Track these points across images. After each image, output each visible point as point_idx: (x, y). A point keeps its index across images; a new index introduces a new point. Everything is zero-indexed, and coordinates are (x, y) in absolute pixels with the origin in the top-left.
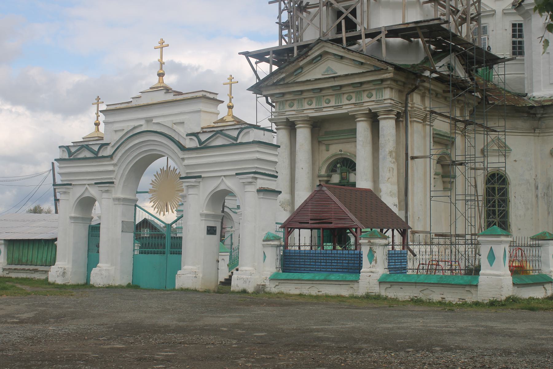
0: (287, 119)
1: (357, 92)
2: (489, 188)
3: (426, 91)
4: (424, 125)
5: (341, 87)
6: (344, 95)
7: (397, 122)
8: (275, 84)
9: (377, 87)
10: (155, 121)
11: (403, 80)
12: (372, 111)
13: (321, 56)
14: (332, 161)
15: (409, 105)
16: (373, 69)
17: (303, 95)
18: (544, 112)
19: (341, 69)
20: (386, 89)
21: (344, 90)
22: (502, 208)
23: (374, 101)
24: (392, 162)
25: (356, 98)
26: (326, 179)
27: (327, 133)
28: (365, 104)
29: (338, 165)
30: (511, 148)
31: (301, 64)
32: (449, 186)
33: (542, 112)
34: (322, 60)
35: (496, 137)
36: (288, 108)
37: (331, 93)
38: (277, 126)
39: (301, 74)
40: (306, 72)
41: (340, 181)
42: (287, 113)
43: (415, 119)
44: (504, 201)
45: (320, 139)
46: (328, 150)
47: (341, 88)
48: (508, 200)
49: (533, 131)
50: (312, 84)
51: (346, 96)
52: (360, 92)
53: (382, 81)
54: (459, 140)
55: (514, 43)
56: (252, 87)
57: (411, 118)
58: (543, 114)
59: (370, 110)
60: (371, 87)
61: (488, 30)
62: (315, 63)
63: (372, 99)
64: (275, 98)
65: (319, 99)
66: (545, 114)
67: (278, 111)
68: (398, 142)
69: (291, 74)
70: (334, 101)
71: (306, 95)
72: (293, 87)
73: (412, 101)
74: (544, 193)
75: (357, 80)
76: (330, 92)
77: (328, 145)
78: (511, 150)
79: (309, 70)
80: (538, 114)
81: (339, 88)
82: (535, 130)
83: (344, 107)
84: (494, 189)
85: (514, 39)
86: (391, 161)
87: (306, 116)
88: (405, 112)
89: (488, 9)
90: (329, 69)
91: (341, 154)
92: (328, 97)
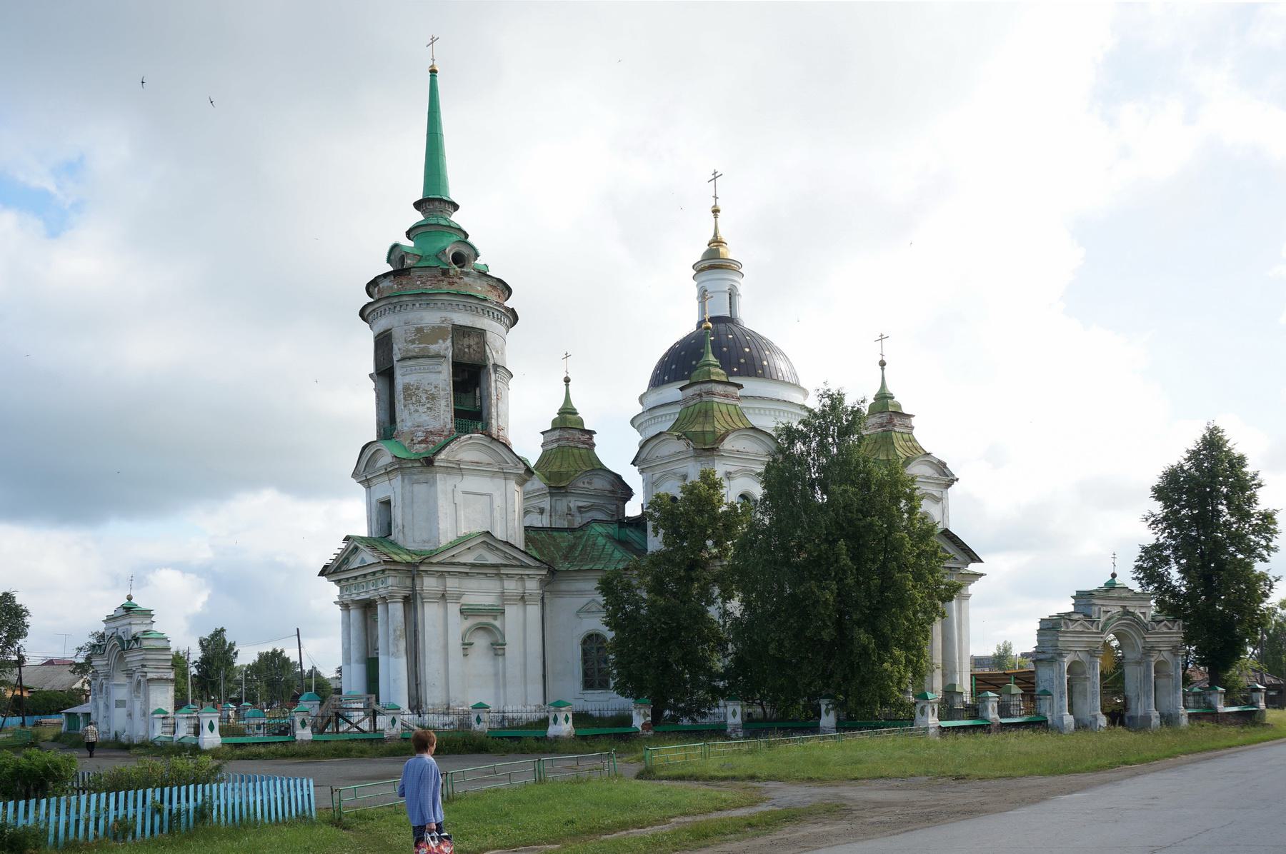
54: (512, 612)
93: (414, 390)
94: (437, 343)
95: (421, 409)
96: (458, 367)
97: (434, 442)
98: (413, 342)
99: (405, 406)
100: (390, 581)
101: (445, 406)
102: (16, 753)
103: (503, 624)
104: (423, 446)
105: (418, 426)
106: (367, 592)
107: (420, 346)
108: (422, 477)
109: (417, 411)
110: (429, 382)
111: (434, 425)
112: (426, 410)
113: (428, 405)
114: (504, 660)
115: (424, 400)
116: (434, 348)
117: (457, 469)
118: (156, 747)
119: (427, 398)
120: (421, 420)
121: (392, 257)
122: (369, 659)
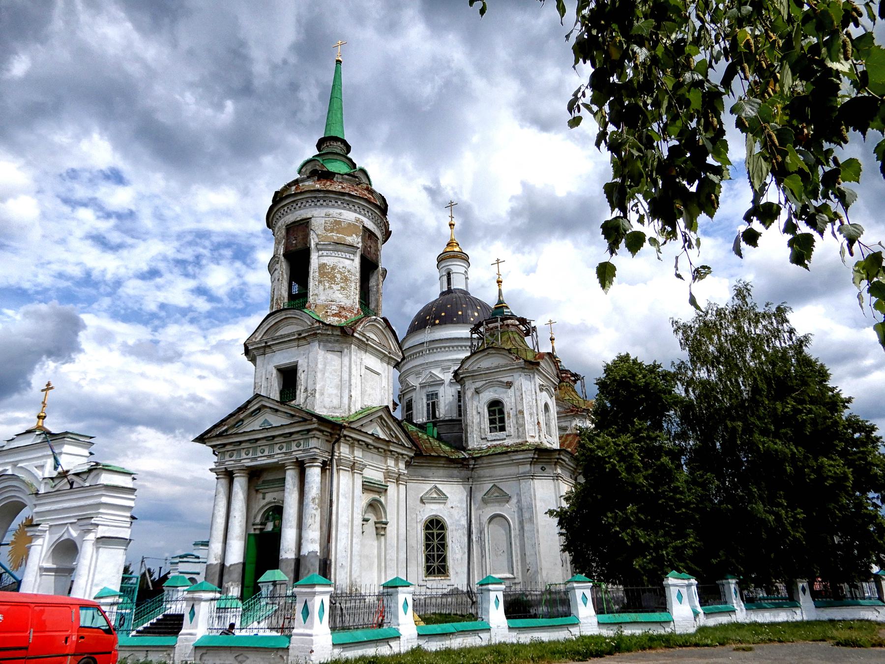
0: (225, 468)
5: (274, 437)
8: (218, 436)
9: (305, 437)
10: (20, 465)
13: (259, 409)
16: (301, 420)
19: (276, 420)
30: (448, 495)
31: (241, 417)
42: (227, 463)
44: (443, 546)
45: (257, 488)
46: (264, 498)
47: (273, 439)
52: (290, 441)
53: (309, 431)
54: (392, 488)
56: (197, 438)
57: (337, 466)
58: (474, 465)
59: (297, 459)
63: (300, 448)
68: (322, 489)
69: (233, 426)
71: (243, 445)
73: (339, 449)
75: (287, 431)
76: (264, 442)
77: (264, 494)
83: (276, 456)
92: (263, 447)
95: (335, 287)
96: (363, 259)
97: (346, 317)
99: (320, 282)
100: (313, 443)
103: (386, 500)
104: (337, 319)
106: (269, 457)
108: (337, 347)
109: (330, 288)
111: (346, 302)
114: (385, 540)
116: (350, 240)
117: (364, 346)
119: (341, 279)
121: (303, 170)
122: (249, 535)
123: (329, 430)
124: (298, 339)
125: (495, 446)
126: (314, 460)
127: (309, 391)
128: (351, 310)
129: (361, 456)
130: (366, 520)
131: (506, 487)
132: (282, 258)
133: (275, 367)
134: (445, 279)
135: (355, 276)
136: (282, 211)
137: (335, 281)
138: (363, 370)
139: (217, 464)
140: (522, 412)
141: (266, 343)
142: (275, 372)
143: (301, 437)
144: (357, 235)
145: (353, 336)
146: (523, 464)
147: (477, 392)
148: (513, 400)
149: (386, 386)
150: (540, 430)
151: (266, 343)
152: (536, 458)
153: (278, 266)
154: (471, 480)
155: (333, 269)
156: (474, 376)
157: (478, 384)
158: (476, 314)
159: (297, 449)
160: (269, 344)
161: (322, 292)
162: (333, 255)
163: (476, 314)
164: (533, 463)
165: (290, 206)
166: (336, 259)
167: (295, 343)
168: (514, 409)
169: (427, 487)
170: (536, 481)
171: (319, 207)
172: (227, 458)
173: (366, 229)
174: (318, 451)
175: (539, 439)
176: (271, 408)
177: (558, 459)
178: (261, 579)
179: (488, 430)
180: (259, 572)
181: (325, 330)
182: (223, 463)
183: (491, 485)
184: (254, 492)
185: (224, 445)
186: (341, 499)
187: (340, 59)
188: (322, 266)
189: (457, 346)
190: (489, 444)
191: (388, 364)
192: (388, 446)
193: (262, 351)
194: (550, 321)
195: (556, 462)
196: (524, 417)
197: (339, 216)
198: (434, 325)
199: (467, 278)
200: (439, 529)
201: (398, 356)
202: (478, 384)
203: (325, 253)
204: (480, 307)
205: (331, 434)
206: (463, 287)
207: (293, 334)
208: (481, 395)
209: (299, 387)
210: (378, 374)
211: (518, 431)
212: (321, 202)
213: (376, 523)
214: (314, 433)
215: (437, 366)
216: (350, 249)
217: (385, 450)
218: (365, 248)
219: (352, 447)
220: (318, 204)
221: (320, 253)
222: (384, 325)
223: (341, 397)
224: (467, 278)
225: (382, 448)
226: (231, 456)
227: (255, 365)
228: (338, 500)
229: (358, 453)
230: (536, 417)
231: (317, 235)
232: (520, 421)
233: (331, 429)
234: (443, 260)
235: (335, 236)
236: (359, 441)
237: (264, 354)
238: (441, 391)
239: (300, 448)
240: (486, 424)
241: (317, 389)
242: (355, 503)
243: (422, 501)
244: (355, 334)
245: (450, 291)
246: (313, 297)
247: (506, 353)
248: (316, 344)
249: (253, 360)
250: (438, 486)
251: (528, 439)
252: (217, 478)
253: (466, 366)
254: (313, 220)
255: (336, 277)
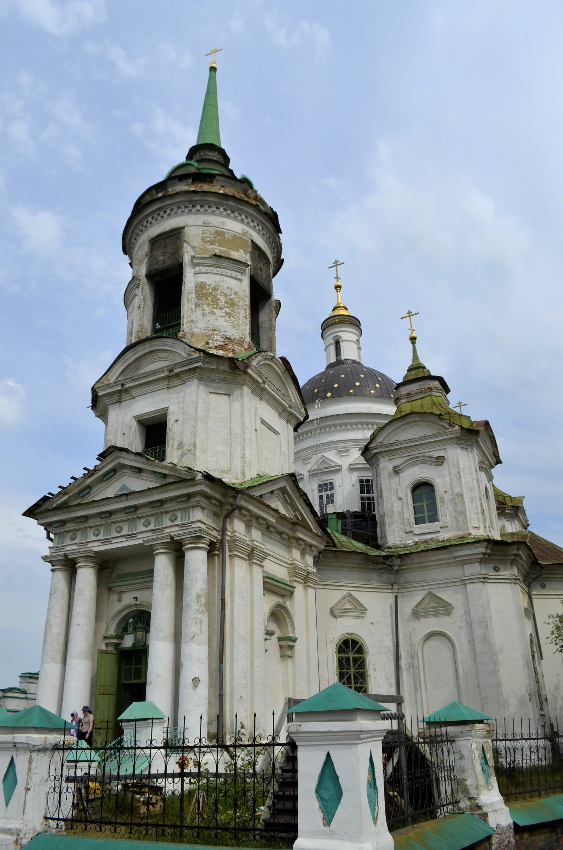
0: (65, 555)
1: (157, 514)
2: (342, 658)
3: (252, 519)
4: (251, 564)
6: (141, 520)
7: (210, 554)
9: (183, 506)
11: (219, 497)
12: (175, 539)
14: (126, 614)
15: (228, 533)
17: (88, 522)
18: (403, 563)
20: (195, 509)
21: (140, 512)
22: (360, 684)
23: (178, 525)
24: (200, 611)
25: (155, 522)
26: (115, 641)
27: (121, 577)
28: (167, 530)
29: (131, 620)
30: (367, 607)
32: (289, 653)
33: (399, 563)
34: (116, 476)
35: (348, 593)
36: (68, 542)
37: (124, 518)
38: (53, 566)
39: (90, 495)
40: (96, 493)
41: (134, 644)
42: (67, 548)
43: (236, 553)
45: (110, 585)
46: (120, 601)
48: (366, 675)
49: (391, 587)
50: (99, 506)
51: (142, 521)
53: (189, 496)
54: (299, 590)
55: (362, 499)
57: (230, 551)
58: (400, 566)
59: (172, 537)
60: (174, 506)
61: (334, 486)
62: (106, 480)
63: (177, 522)
64: (54, 529)
65: (107, 526)
66: (403, 565)
67: (56, 545)
70: (127, 529)
71: (92, 522)
72: (75, 511)
74: (410, 663)
76: (122, 516)
78: (366, 610)
79: (100, 490)
80: (395, 566)
81: (133, 510)
82: (392, 586)
83: (139, 536)
84: (348, 659)
85: (363, 495)
86: (198, 610)
87: (89, 550)
88: (222, 542)
89: (333, 464)
90: (124, 487)
91: (136, 605)
92: (120, 524)
93: (210, 291)
94: (238, 251)
95: (218, 312)
98: (212, 243)
99: (197, 305)
100: (198, 515)
101: (244, 317)
102: (347, 678)
105: (213, 330)
107: (221, 248)
109: (212, 313)
110: (230, 286)
112: (224, 314)
113: (227, 310)
115: (222, 303)
116: (235, 255)
118: (552, 743)
119: (226, 302)
120: (217, 324)
123: (219, 497)
124: (168, 378)
125: (426, 542)
126: (199, 538)
127: (186, 447)
128: (240, 343)
129: (260, 540)
130: (269, 633)
131: (445, 595)
132: (144, 280)
133: (135, 417)
134: (332, 348)
135: (244, 301)
136: (145, 223)
137: (218, 304)
138: (259, 426)
139: (53, 551)
140: (461, 495)
141: (123, 385)
142: (135, 424)
143: (178, 507)
144: (244, 251)
145: (246, 372)
146: (470, 562)
147: (397, 471)
148: (448, 480)
149: (286, 451)
150: (484, 522)
151: (123, 385)
152: (489, 555)
153: (138, 291)
154: (395, 587)
155: (215, 289)
156: (390, 452)
157: (397, 462)
158: (378, 386)
159: (172, 524)
160: (126, 386)
161: (200, 317)
162: (215, 272)
163: (378, 386)
164: (484, 560)
165: (155, 216)
166: (219, 278)
167: (164, 384)
168: (449, 492)
169: (337, 595)
170: (489, 586)
171: (195, 214)
172: (68, 542)
173: (255, 246)
174: (203, 526)
175: (485, 531)
176: (132, 467)
177: (516, 555)
178: (125, 716)
179: (413, 521)
180: (121, 708)
181: (208, 363)
182: (61, 548)
183: (424, 593)
184: (106, 593)
185: (63, 523)
186: (237, 599)
187: (214, 65)
188: (200, 287)
189: (357, 424)
190: (416, 539)
191: (288, 422)
192: (294, 531)
193: (116, 397)
194: (460, 403)
195: (513, 560)
196: (463, 502)
197: (220, 226)
198: (325, 398)
199: (359, 348)
200: (355, 653)
201: (300, 413)
202: (397, 462)
203: (204, 269)
204: (381, 378)
205: (221, 504)
206: (355, 358)
207: (161, 370)
208: (401, 475)
209: (171, 443)
210: (276, 432)
211: (458, 521)
212: (198, 207)
213: (280, 639)
214: (197, 499)
215: (332, 449)
216: (237, 266)
217: (289, 538)
218: (254, 269)
219: (248, 526)
220: (194, 210)
221: (197, 269)
222: (283, 368)
223: (231, 456)
224: (359, 348)
225: (286, 534)
226: (73, 539)
227: (106, 422)
228: (232, 600)
229: (256, 535)
230: (479, 503)
231: (193, 247)
232: (460, 508)
233: (222, 495)
234: (324, 329)
235: (218, 249)
236: (258, 518)
237: (119, 402)
238: (337, 479)
239: (177, 522)
240: (410, 514)
241: (197, 443)
242: (255, 608)
243: (333, 613)
244: (249, 371)
245: (339, 362)
246: (188, 325)
247: (436, 419)
248: (195, 382)
249: (103, 415)
250: (353, 593)
251: (471, 531)
252: (53, 571)
253: (380, 439)
254: (187, 230)
255: (219, 299)
